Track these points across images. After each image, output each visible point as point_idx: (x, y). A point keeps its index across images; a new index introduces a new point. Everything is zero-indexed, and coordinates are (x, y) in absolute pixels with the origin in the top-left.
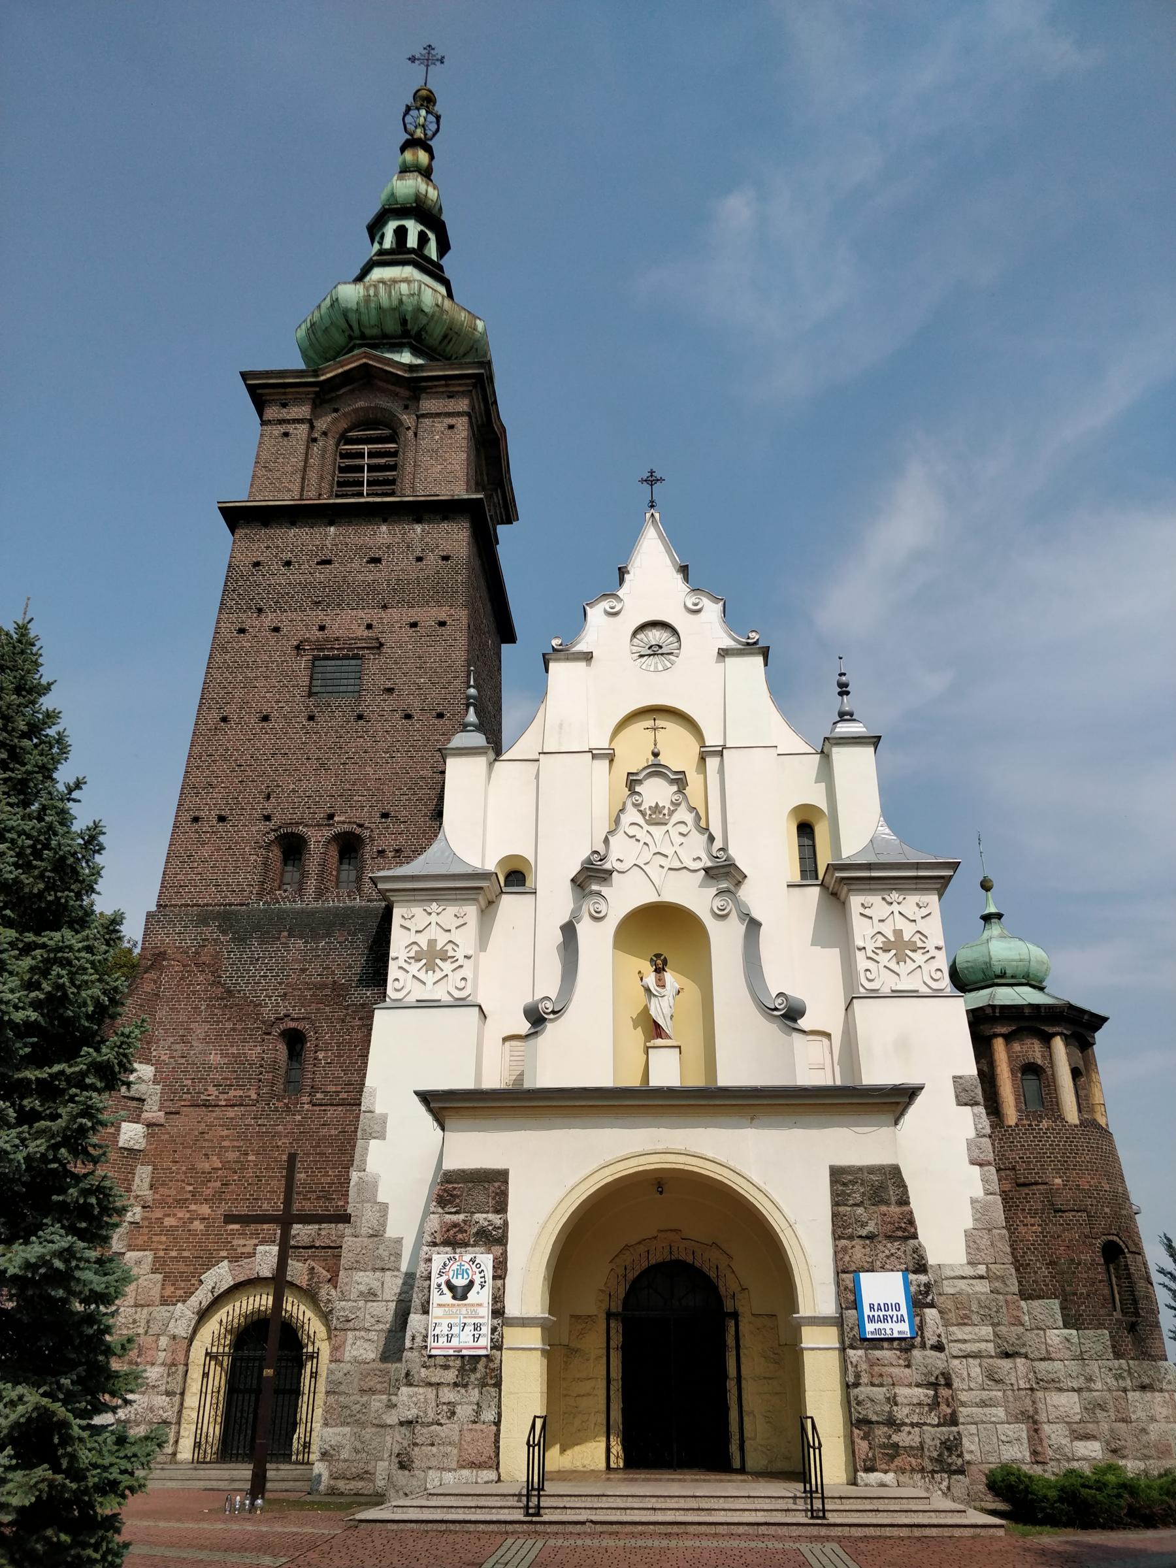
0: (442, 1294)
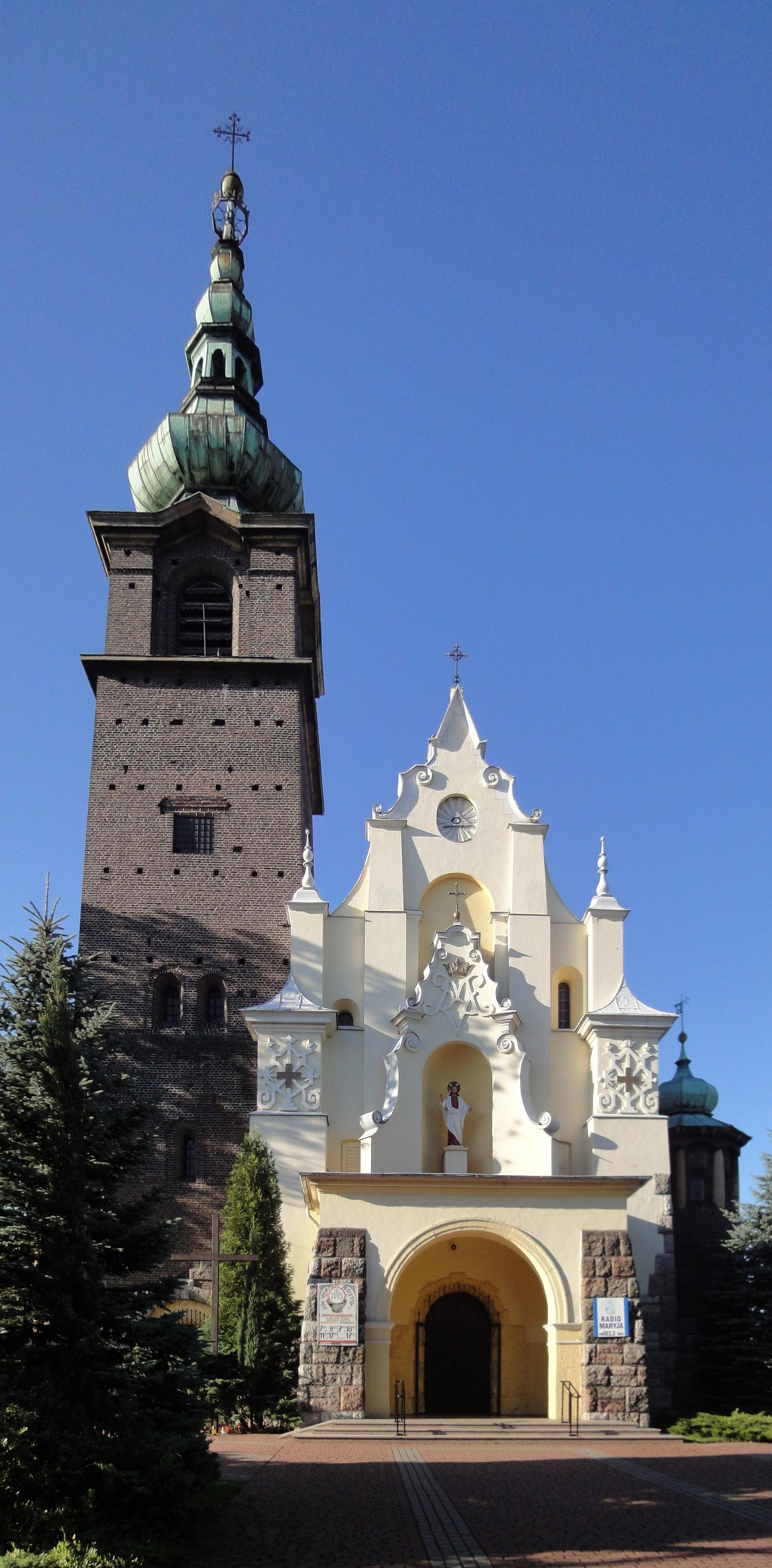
0: (325, 1308)
